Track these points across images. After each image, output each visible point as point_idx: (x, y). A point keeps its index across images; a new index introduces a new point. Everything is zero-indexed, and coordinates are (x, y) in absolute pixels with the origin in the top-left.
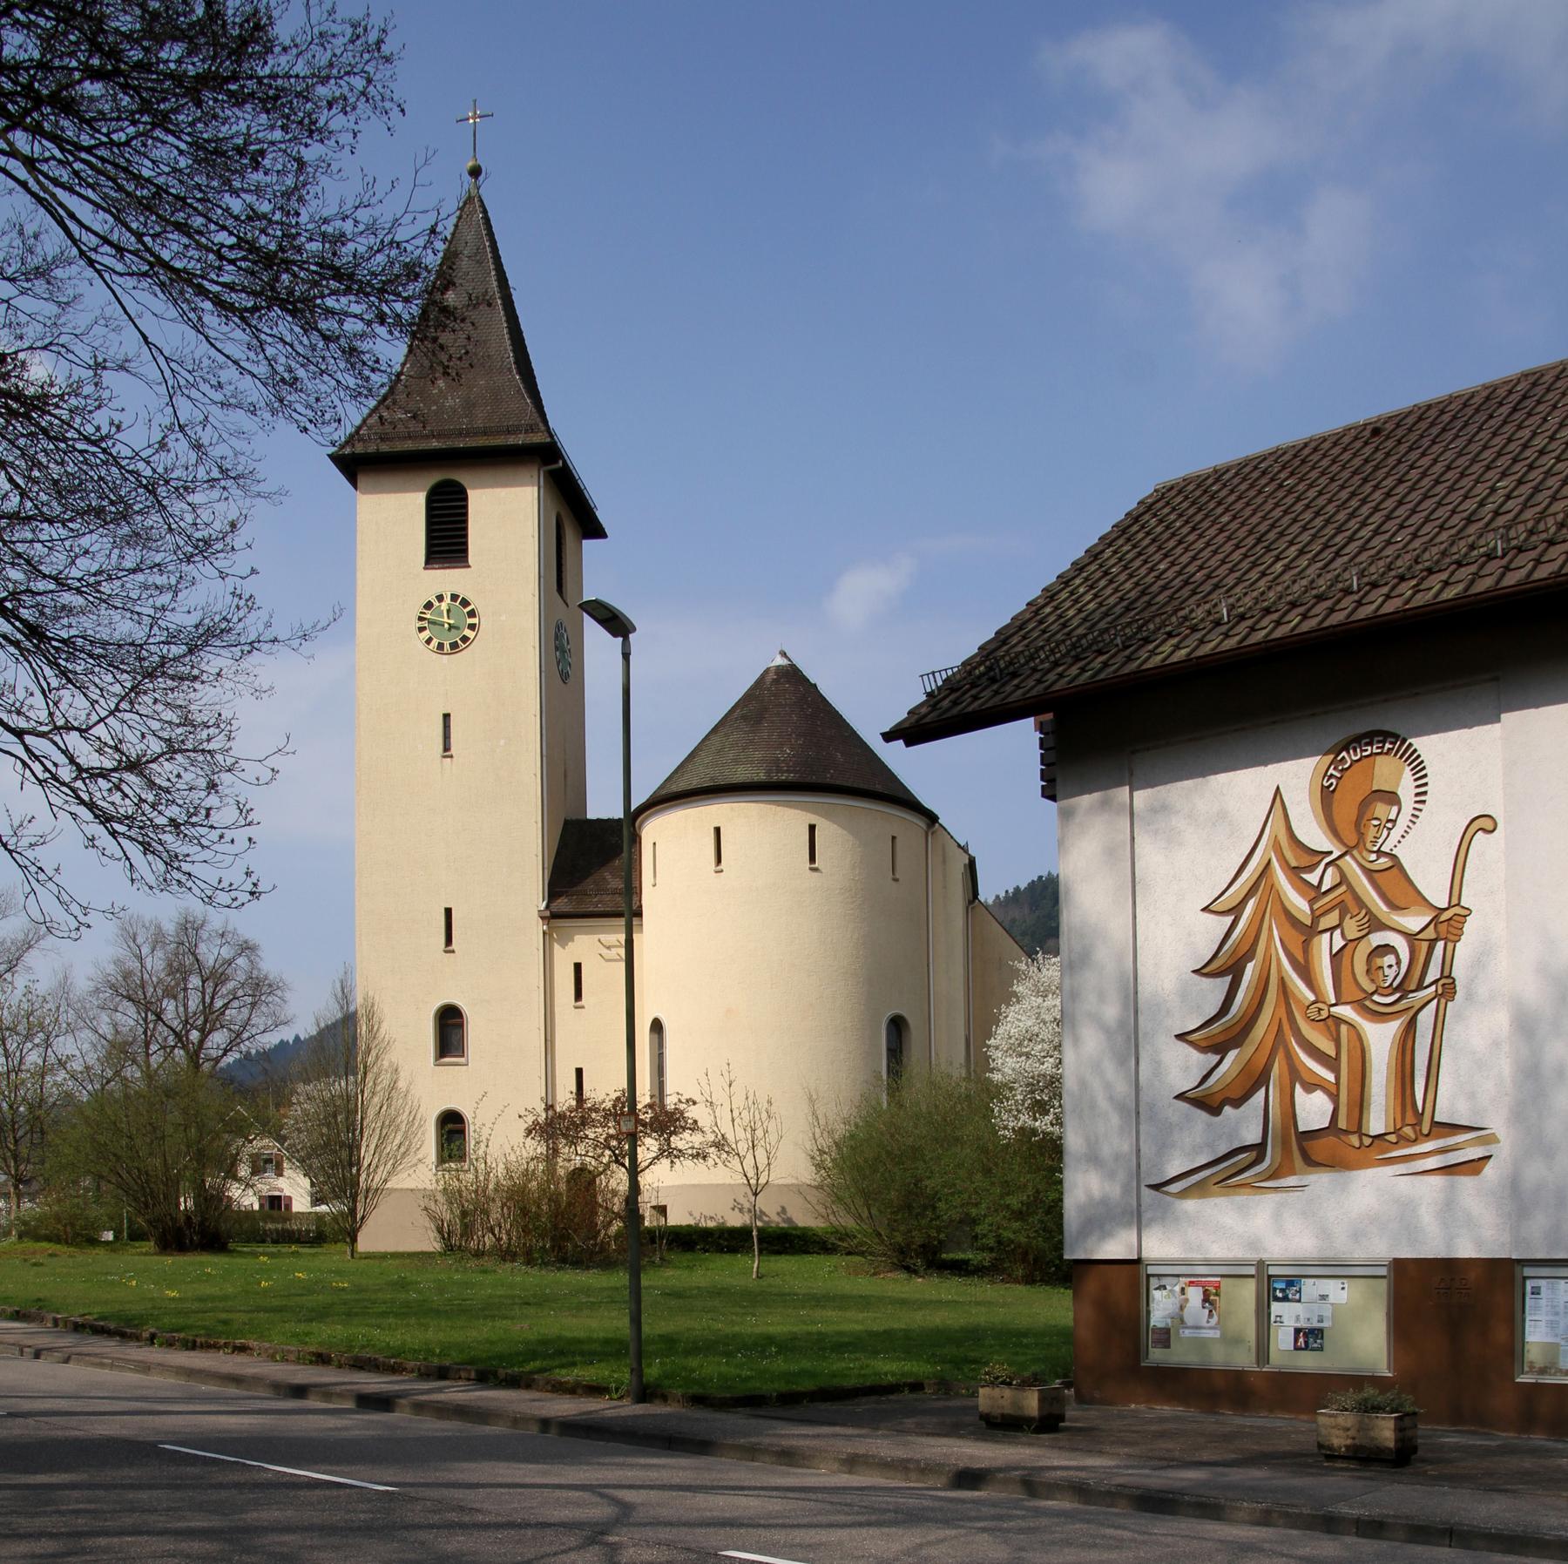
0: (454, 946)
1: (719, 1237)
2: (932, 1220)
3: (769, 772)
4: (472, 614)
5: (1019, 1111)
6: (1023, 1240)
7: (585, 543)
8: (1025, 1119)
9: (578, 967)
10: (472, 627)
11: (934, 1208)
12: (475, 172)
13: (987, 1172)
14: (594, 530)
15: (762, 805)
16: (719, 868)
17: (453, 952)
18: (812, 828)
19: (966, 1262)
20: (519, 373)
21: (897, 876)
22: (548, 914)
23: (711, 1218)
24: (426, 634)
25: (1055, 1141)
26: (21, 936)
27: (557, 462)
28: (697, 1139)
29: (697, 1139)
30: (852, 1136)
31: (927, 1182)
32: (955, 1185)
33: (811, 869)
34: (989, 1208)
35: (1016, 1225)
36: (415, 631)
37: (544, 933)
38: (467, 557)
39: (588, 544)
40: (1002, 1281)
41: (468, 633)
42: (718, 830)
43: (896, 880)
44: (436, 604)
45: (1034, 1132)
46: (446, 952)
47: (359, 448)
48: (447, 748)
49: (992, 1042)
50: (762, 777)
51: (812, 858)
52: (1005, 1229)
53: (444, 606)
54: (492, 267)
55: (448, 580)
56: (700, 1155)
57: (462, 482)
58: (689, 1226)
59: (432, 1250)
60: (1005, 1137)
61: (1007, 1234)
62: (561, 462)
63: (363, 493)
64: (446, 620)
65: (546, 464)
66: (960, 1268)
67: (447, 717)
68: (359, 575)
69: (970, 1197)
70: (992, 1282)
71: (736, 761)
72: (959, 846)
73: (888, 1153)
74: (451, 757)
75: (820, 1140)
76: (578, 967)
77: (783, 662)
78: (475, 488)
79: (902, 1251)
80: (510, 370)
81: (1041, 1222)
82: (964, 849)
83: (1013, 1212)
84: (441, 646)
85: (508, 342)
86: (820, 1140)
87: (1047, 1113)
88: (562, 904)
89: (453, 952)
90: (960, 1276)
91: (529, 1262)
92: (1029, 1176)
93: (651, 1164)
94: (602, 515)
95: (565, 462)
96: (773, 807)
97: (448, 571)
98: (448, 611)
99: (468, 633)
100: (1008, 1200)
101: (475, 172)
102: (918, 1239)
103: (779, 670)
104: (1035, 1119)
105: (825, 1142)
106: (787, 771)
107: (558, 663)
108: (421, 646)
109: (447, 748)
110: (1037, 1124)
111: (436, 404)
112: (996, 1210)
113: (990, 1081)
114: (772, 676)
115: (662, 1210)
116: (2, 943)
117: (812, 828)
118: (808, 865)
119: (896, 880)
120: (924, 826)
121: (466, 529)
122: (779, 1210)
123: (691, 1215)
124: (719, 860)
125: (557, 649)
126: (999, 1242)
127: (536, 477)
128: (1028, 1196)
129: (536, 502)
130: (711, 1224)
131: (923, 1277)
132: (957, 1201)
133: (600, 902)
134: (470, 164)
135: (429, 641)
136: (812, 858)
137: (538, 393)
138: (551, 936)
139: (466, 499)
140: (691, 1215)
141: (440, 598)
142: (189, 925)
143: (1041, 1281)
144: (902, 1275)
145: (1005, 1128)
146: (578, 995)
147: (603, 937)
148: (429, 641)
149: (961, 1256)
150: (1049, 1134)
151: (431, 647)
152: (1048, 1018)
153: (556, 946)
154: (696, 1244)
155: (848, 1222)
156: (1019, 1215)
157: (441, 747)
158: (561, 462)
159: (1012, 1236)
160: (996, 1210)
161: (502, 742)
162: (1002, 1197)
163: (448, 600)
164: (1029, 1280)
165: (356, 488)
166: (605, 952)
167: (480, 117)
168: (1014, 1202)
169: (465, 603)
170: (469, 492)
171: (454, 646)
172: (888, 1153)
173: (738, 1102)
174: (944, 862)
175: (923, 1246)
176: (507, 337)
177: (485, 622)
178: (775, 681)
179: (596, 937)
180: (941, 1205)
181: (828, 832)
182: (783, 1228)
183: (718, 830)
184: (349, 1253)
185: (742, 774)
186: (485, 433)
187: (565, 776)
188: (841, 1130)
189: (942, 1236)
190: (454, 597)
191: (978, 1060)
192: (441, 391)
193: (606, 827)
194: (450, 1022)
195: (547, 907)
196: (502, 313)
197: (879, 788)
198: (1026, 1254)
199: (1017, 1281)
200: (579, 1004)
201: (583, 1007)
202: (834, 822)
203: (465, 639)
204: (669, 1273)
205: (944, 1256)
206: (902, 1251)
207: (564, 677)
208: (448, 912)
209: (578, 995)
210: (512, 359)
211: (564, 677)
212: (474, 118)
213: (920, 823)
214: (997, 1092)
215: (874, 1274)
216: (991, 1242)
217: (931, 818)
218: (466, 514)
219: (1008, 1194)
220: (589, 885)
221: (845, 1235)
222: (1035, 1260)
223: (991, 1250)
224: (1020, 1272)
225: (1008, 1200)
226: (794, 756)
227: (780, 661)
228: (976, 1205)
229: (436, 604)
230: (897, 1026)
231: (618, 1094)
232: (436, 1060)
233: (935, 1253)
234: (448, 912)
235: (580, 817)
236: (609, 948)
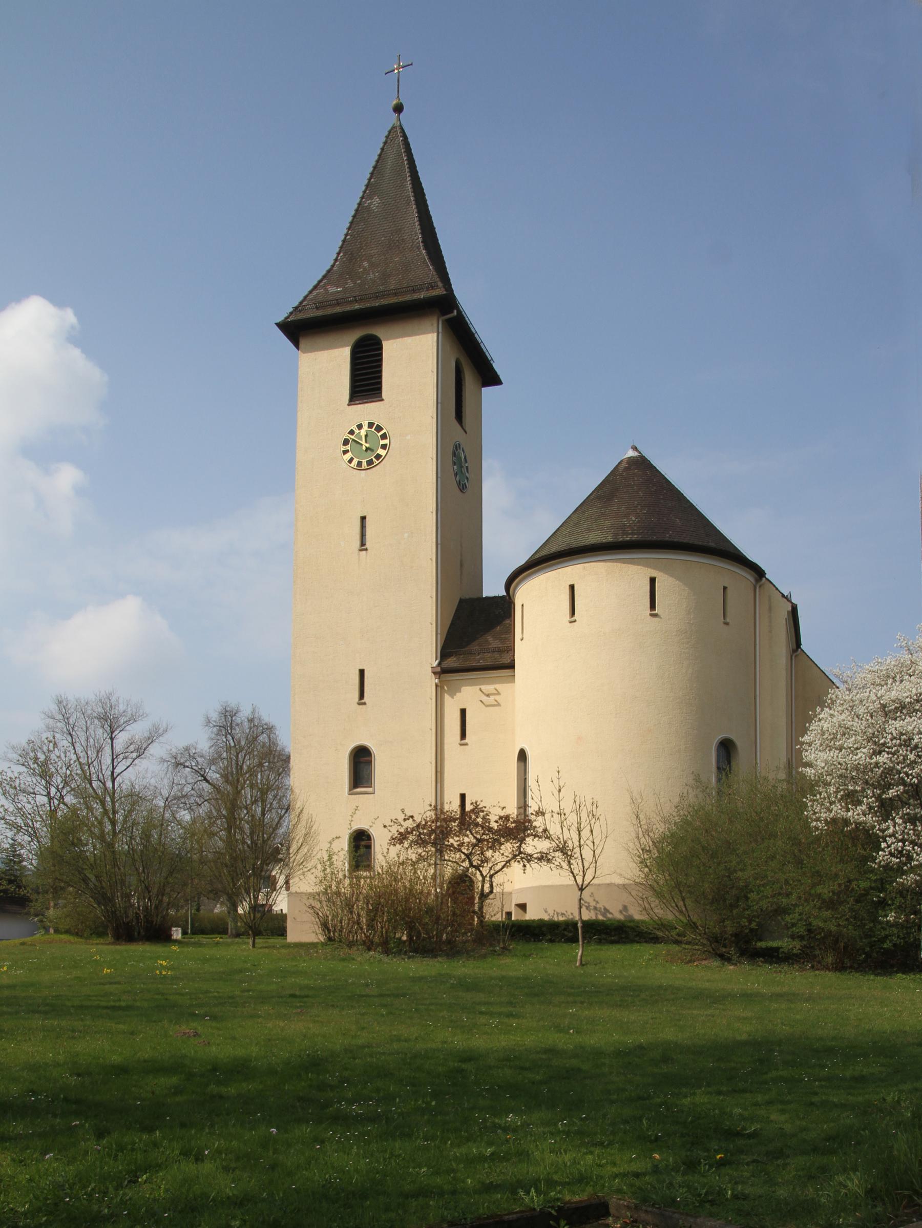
0: (366, 699)
1: (565, 929)
2: (744, 909)
3: (616, 535)
4: (384, 437)
5: (831, 803)
6: (834, 929)
7: (483, 389)
8: (837, 810)
9: (463, 712)
10: (384, 447)
11: (747, 898)
12: (398, 109)
13: (799, 863)
14: (490, 378)
15: (609, 564)
16: (573, 619)
17: (365, 704)
18: (653, 581)
19: (777, 949)
20: (426, 248)
21: (728, 620)
22: (439, 669)
23: (563, 914)
24: (348, 456)
25: (868, 831)
26: (147, 734)
27: (452, 312)
28: (543, 845)
29: (543, 845)
30: (673, 835)
31: (740, 874)
32: (766, 876)
33: (651, 615)
34: (800, 898)
35: (828, 914)
36: (340, 453)
37: (437, 686)
38: (381, 393)
39: (486, 391)
40: (813, 967)
41: (382, 452)
42: (572, 587)
43: (727, 624)
44: (357, 431)
45: (846, 822)
46: (359, 704)
47: (300, 316)
48: (363, 543)
49: (806, 738)
50: (610, 539)
51: (653, 606)
52: (815, 917)
53: (363, 432)
54: (408, 174)
55: (368, 412)
56: (543, 858)
57: (377, 335)
58: (541, 920)
59: (316, 941)
60: (817, 828)
61: (817, 923)
62: (455, 312)
63: (304, 352)
64: (363, 442)
65: (444, 315)
66: (772, 956)
67: (363, 519)
68: (299, 414)
69: (781, 888)
70: (802, 969)
71: (589, 530)
72: (783, 596)
73: (703, 848)
74: (366, 550)
75: (643, 840)
76: (463, 712)
77: (635, 454)
78: (388, 339)
79: (716, 939)
80: (418, 248)
81: (851, 910)
82: (787, 598)
83: (824, 901)
84: (360, 464)
85: (418, 227)
86: (643, 840)
87: (860, 803)
88: (451, 662)
89: (365, 704)
90: (771, 964)
91: (387, 952)
92: (840, 867)
93: (503, 867)
94: (496, 366)
95: (459, 312)
96: (619, 564)
97: (366, 405)
98: (366, 436)
99: (382, 452)
100: (819, 889)
101: (398, 109)
102: (730, 927)
103: (631, 461)
104: (848, 810)
105: (646, 842)
106: (632, 534)
107: (456, 475)
108: (345, 465)
109: (363, 543)
110: (850, 814)
111: (360, 279)
112: (806, 900)
113: (803, 776)
114: (624, 465)
115: (523, 907)
116: (920, 971)
117: (653, 581)
118: (648, 612)
119: (727, 624)
120: (752, 580)
121: (381, 371)
122: (621, 908)
123: (546, 912)
124: (573, 613)
125: (454, 464)
126: (809, 931)
127: (435, 325)
128: (840, 885)
129: (435, 344)
130: (561, 919)
131: (736, 965)
132: (768, 891)
133: (481, 659)
134: (395, 102)
135: (351, 461)
136: (653, 606)
137: (443, 263)
138: (442, 688)
139: (381, 348)
140: (546, 912)
141: (360, 427)
142: (228, 714)
143: (851, 967)
144: (715, 963)
145: (818, 820)
146: (463, 735)
147: (483, 687)
148: (351, 461)
149: (774, 944)
150: (860, 823)
151: (352, 465)
152: (861, 710)
153: (447, 697)
154: (544, 935)
155: (669, 915)
156: (831, 904)
157: (358, 543)
158: (455, 312)
159: (821, 925)
160: (806, 900)
161: (406, 535)
162: (814, 886)
163: (365, 427)
164: (840, 967)
165: (298, 348)
166: (485, 698)
167: (402, 67)
168: (825, 891)
169: (379, 429)
170: (384, 343)
171: (370, 462)
172: (703, 848)
173: (567, 806)
174: (770, 609)
175: (736, 935)
176: (417, 224)
177: (394, 442)
178: (626, 469)
179: (478, 687)
180: (752, 896)
181: (665, 583)
182: (619, 921)
183: (572, 587)
184: (251, 943)
185: (593, 538)
186: (396, 294)
187: (461, 565)
188: (660, 828)
189: (753, 925)
190: (371, 425)
191: (794, 760)
192: (365, 269)
193: (494, 601)
194: (362, 759)
195: (439, 664)
196: (414, 206)
197: (712, 544)
198: (836, 941)
199: (827, 968)
200: (463, 742)
201: (466, 744)
202: (672, 576)
203: (378, 457)
204: (506, 961)
205: (759, 944)
206: (716, 939)
207: (462, 488)
208: (362, 672)
209: (463, 735)
210: (420, 240)
211: (462, 488)
212: (398, 68)
213: (748, 576)
214: (810, 787)
215: (690, 961)
216: (801, 930)
217: (759, 573)
218: (381, 360)
219: (819, 884)
220: (474, 647)
221: (663, 925)
222: (845, 947)
223: (801, 938)
224: (830, 959)
225: (819, 889)
226: (638, 522)
227: (631, 453)
228: (788, 895)
229: (357, 431)
230: (727, 748)
231: (638, 869)
232: (350, 790)
233: (748, 942)
234: (362, 672)
235: (474, 595)
236: (488, 695)
